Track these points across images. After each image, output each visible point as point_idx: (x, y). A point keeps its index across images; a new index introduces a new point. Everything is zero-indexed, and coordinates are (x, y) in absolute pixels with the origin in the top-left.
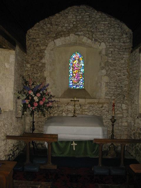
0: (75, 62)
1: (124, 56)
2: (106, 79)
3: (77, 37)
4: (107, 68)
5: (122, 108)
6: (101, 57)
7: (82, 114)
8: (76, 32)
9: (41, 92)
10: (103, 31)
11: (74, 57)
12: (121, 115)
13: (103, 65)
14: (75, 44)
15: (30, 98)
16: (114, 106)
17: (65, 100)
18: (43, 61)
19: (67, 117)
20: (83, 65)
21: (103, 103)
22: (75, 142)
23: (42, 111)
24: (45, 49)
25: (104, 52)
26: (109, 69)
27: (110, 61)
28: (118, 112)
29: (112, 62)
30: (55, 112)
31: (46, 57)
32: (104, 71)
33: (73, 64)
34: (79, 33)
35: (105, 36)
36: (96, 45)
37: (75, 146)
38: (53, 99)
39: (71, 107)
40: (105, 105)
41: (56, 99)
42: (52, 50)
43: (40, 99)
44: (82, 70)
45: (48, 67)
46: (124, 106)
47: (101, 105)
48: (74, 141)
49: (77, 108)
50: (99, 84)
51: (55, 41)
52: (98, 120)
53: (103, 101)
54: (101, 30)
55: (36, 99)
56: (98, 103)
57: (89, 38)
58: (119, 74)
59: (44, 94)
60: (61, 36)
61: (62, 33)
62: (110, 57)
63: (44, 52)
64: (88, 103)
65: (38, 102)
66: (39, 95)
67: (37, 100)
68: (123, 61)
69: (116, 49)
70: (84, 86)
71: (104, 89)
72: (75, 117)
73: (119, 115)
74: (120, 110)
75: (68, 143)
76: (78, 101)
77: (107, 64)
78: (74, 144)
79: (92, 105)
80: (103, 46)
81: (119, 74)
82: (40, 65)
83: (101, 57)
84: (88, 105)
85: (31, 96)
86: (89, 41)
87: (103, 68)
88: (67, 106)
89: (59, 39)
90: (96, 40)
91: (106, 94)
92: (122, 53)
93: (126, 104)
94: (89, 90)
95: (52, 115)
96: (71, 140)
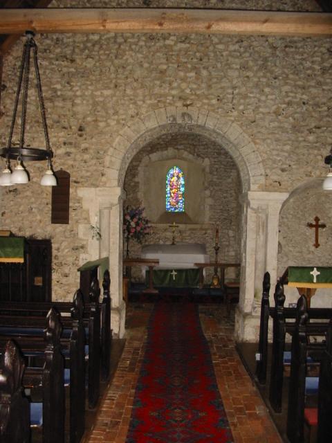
0: (174, 178)
1: (232, 174)
2: (209, 201)
3: (176, 151)
4: (212, 189)
5: (228, 235)
6: (205, 175)
7: (182, 242)
8: (176, 145)
9: (137, 217)
10: (206, 144)
11: (172, 173)
12: (227, 243)
13: (206, 184)
14: (175, 158)
15: (127, 223)
16: (217, 232)
17: (162, 225)
18: (136, 180)
19: (164, 245)
20: (183, 183)
21: (206, 230)
22: (175, 271)
23: (139, 238)
24: (138, 166)
25: (208, 170)
26: (214, 189)
27: (215, 180)
28: (224, 239)
29: (218, 181)
30: (151, 240)
31: (139, 175)
32: (208, 192)
33: (170, 181)
34: (179, 147)
35: (209, 150)
36: (200, 161)
37: (176, 275)
38: (149, 225)
39: (169, 234)
40: (209, 232)
41: (153, 225)
42: (147, 166)
43: (137, 224)
44: (182, 189)
45: (142, 188)
46: (231, 233)
47: (204, 232)
48: (313, 282)
49: (176, 234)
50: (202, 207)
51: (151, 156)
52: (202, 248)
53: (207, 227)
54: (205, 143)
55: (133, 224)
56: (201, 229)
57: (190, 153)
58: (225, 195)
59: (139, 219)
60: (158, 149)
61: (159, 146)
62: (214, 175)
63: (137, 169)
64: (190, 229)
65: (135, 228)
66: (135, 220)
67: (134, 226)
68: (230, 180)
69: (222, 166)
70: (184, 208)
71: (208, 213)
72: (174, 246)
73: (224, 243)
74: (227, 236)
75: (167, 271)
76: (177, 227)
77: (211, 183)
78: (38, 281)
79: (194, 232)
80: (207, 162)
81: (225, 195)
82: (132, 184)
83: (205, 175)
84: (188, 232)
85: (128, 221)
86: (191, 156)
87: (206, 189)
88: (165, 233)
89: (155, 154)
90: (198, 156)
91: (211, 219)
92: (229, 170)
93: (233, 230)
94: (190, 214)
95: (147, 243)
96: (171, 269)
